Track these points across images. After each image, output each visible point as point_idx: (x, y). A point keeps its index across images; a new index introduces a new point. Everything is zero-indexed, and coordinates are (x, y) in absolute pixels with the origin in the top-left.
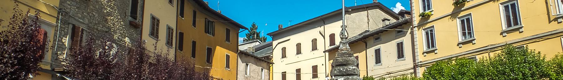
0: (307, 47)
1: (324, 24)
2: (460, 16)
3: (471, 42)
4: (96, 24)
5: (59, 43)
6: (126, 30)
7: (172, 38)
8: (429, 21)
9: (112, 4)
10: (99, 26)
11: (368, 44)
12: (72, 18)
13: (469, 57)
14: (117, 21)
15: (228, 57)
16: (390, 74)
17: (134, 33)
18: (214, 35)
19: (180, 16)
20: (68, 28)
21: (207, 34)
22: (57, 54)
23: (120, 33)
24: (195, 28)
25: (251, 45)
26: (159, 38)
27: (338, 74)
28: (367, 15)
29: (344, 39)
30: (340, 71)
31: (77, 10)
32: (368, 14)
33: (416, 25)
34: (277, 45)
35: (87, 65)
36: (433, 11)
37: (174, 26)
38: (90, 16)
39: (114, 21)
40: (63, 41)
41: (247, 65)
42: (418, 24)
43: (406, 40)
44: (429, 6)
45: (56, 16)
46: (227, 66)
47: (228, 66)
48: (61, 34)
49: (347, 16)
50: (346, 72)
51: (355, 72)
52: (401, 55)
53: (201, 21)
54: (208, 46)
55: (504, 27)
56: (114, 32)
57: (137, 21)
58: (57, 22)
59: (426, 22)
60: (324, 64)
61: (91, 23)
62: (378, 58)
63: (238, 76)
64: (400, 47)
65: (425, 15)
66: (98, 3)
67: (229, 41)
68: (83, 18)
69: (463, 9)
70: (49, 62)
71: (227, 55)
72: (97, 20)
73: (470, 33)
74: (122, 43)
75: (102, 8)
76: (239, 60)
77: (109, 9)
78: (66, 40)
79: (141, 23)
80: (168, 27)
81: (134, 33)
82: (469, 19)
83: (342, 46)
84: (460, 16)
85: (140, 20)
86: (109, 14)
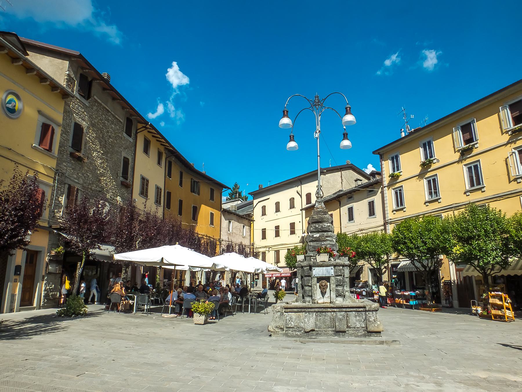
0: (285, 205)
2: (426, 176)
4: (90, 184)
5: (56, 201)
6: (117, 189)
7: (160, 197)
8: (398, 181)
11: (341, 202)
14: (109, 182)
15: (212, 215)
16: (362, 230)
18: (199, 194)
19: (168, 177)
20: (64, 187)
21: (193, 193)
22: (54, 212)
23: (113, 193)
24: (182, 188)
29: (320, 198)
30: (316, 228)
31: (72, 171)
33: (386, 185)
34: (257, 204)
35: (81, 222)
37: (162, 186)
41: (230, 222)
42: (388, 184)
43: (377, 199)
44: (398, 167)
45: (53, 177)
51: (329, 229)
53: (187, 181)
54: (194, 204)
55: (468, 187)
56: (107, 191)
57: (128, 181)
58: (54, 182)
59: (395, 182)
61: (85, 183)
64: (371, 205)
67: (213, 200)
68: (78, 178)
69: (429, 170)
73: (436, 193)
74: (114, 202)
75: (96, 169)
76: (223, 217)
77: (102, 170)
79: (131, 183)
82: (435, 180)
84: (426, 176)
86: (102, 175)
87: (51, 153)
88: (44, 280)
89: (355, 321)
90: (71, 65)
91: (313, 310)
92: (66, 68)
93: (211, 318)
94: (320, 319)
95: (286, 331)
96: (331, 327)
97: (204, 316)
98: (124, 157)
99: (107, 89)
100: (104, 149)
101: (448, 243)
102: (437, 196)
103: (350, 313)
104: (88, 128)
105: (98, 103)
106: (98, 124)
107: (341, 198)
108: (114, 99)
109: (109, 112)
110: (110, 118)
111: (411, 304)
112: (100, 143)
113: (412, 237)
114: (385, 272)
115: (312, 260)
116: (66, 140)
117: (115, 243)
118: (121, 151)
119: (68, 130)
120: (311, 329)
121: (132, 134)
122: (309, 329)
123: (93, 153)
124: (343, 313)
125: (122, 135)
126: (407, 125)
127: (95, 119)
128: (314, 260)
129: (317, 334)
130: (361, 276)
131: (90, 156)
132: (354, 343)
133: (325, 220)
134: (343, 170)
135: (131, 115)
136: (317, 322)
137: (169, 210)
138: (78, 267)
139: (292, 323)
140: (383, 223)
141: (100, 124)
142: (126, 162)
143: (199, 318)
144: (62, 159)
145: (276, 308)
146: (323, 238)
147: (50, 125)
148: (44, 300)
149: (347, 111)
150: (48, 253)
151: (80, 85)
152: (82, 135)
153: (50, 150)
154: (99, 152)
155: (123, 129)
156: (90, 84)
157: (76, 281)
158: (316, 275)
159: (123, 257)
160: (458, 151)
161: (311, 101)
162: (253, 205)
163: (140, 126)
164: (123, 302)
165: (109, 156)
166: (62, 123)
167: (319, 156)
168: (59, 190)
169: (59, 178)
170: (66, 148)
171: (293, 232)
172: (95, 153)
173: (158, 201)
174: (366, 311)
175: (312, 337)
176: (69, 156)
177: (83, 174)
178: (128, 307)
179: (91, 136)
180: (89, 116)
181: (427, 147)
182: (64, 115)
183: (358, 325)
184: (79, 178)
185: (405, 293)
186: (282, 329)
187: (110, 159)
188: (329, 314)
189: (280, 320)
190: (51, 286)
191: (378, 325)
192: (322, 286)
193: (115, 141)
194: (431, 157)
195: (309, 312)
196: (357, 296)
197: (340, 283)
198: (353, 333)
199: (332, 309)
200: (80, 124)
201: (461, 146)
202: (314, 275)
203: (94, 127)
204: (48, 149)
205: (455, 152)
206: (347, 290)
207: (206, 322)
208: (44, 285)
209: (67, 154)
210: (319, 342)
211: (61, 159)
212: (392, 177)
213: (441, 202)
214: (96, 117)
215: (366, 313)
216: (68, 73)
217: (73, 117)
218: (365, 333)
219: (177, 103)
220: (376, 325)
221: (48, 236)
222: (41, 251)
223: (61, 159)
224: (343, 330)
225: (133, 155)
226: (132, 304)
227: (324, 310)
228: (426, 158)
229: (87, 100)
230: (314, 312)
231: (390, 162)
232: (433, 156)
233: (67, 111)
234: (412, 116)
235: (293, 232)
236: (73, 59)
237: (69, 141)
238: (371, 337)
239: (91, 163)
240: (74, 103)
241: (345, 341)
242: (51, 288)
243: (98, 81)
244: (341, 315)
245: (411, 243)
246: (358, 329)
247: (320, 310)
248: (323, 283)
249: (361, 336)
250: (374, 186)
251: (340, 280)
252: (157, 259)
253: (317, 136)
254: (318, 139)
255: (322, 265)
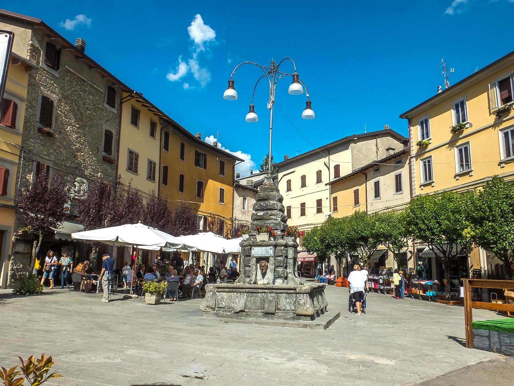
0: (311, 179)
1: (329, 154)
2: (458, 144)
3: (467, 173)
4: (64, 160)
5: (23, 179)
6: (98, 165)
7: (154, 173)
8: (427, 150)
9: (82, 141)
10: (67, 163)
11: (368, 176)
12: (36, 156)
13: (458, 190)
14: (88, 157)
15: (222, 191)
16: (389, 208)
17: (109, 168)
18: (205, 167)
19: (164, 150)
20: (32, 165)
21: (198, 167)
22: (20, 190)
23: (92, 169)
24: (184, 161)
25: (259, 177)
26: (138, 173)
27: (259, 208)
28: (376, 144)
29: (269, 174)
30: (261, 206)
31: (41, 147)
32: (377, 143)
33: (414, 155)
34: (282, 177)
35: (36, 201)
36: (431, 139)
37: (156, 160)
38: (57, 153)
39: (85, 157)
40: (28, 178)
41: (245, 199)
42: (416, 154)
43: (404, 171)
44: (427, 133)
45: (19, 154)
46: (220, 201)
47: (222, 200)
48: (25, 171)
49: (353, 146)
50: (266, 206)
51: (274, 207)
52: (399, 188)
53: (190, 154)
54: (198, 179)
55: (503, 157)
56: (85, 168)
57: (112, 155)
58: (20, 160)
59: (423, 152)
60: (329, 198)
61: (58, 159)
62: (377, 192)
63: (234, 211)
64: (398, 178)
65: (422, 144)
66: (66, 140)
67: (223, 174)
68: (49, 154)
69: (460, 137)
70: (12, 198)
71: (221, 189)
72: (65, 156)
73: (467, 165)
74: (94, 178)
75: (70, 145)
76: (236, 193)
77: (78, 145)
78: (31, 177)
79: (116, 158)
80: (149, 161)
81: (109, 168)
82: (468, 148)
83: (266, 181)
84: (458, 144)
85: (116, 155)
86: (79, 150)
87: (14, 130)
88: (10, 260)
89: (285, 303)
90: (34, 34)
91: (244, 290)
92: (29, 37)
93: (172, 299)
94: (250, 300)
95: (217, 311)
96: (261, 309)
97: (155, 296)
98: (106, 130)
99: (80, 58)
100: (80, 123)
101: (460, 225)
102: (469, 168)
103: (281, 295)
104: (60, 101)
105: (71, 73)
106: (71, 96)
107: (367, 170)
108: (90, 67)
109: (85, 82)
110: (87, 89)
111: (427, 295)
112: (75, 115)
113: (424, 216)
114: (411, 258)
115: (252, 239)
116: (32, 115)
117: (84, 221)
118: (102, 124)
119: (35, 105)
120: (241, 309)
121: (116, 105)
122: (238, 309)
123: (67, 128)
124: (274, 294)
125: (103, 106)
126: (446, 81)
127: (68, 91)
128: (254, 239)
129: (246, 315)
130: (386, 262)
131: (63, 131)
132: (278, 325)
133: (271, 197)
134: (378, 136)
135: (113, 84)
136: (248, 303)
137: (167, 186)
138: (35, 246)
139: (223, 303)
140: (410, 200)
141: (74, 96)
142: (109, 136)
143: (150, 298)
144: (28, 135)
145: (209, 288)
146: (267, 216)
147: (12, 100)
148: (11, 280)
149: (294, 78)
150: (15, 232)
151: (47, 55)
152: (52, 109)
153: (13, 126)
154: (74, 126)
155: (104, 99)
156: (58, 53)
157: (33, 260)
158: (255, 255)
159: (80, 236)
160: (494, 113)
161: (264, 68)
162: (278, 180)
163: (125, 94)
164: (84, 282)
165: (87, 129)
166: (26, 98)
167: (271, 129)
168: (27, 168)
169: (24, 154)
170: (33, 123)
171: (319, 211)
172: (69, 127)
173: (151, 177)
174: (296, 293)
175: (241, 318)
176: (37, 131)
177: (54, 151)
178: (90, 287)
179: (64, 109)
180: (59, 88)
181: (460, 108)
182: (28, 89)
183: (288, 308)
184: (50, 155)
185: (421, 282)
186: (213, 309)
187: (88, 132)
188: (260, 295)
189: (211, 299)
190: (18, 266)
191: (307, 308)
192: (261, 266)
193: (95, 114)
194: (464, 120)
195: (240, 292)
196: (374, 284)
197: (280, 263)
198: (282, 316)
199: (263, 290)
200: (48, 97)
201: (497, 106)
202: (253, 255)
203: (66, 99)
204: (10, 126)
205: (490, 114)
206: (290, 271)
207: (157, 303)
208: (10, 265)
209: (35, 130)
210: (248, 323)
211: (27, 136)
212: (420, 145)
213: (472, 175)
214: (69, 89)
215: (296, 295)
216: (31, 43)
217: (40, 90)
218: (294, 316)
219: (202, 61)
220: (305, 308)
221: (14, 215)
222: (7, 230)
223: (27, 136)
224: (271, 311)
225: (117, 127)
226: (96, 284)
227: (255, 291)
228: (458, 122)
229: (57, 70)
230: (246, 292)
231: (419, 127)
232: (466, 120)
233: (32, 84)
234: (452, 70)
235: (319, 211)
236: (36, 27)
237: (36, 116)
238: (300, 321)
239: (64, 138)
240: (40, 75)
241: (268, 322)
242: (18, 267)
243: (68, 49)
244: (272, 296)
245: (423, 224)
246: (287, 311)
247: (251, 290)
248: (263, 263)
249: (289, 319)
250: (401, 156)
251: (280, 261)
252: (112, 238)
253: (270, 107)
254: (271, 110)
255: (261, 245)
